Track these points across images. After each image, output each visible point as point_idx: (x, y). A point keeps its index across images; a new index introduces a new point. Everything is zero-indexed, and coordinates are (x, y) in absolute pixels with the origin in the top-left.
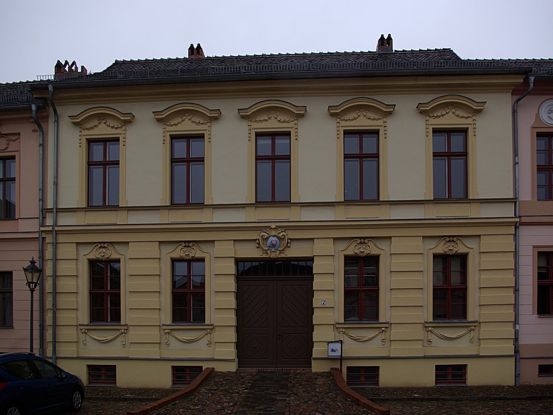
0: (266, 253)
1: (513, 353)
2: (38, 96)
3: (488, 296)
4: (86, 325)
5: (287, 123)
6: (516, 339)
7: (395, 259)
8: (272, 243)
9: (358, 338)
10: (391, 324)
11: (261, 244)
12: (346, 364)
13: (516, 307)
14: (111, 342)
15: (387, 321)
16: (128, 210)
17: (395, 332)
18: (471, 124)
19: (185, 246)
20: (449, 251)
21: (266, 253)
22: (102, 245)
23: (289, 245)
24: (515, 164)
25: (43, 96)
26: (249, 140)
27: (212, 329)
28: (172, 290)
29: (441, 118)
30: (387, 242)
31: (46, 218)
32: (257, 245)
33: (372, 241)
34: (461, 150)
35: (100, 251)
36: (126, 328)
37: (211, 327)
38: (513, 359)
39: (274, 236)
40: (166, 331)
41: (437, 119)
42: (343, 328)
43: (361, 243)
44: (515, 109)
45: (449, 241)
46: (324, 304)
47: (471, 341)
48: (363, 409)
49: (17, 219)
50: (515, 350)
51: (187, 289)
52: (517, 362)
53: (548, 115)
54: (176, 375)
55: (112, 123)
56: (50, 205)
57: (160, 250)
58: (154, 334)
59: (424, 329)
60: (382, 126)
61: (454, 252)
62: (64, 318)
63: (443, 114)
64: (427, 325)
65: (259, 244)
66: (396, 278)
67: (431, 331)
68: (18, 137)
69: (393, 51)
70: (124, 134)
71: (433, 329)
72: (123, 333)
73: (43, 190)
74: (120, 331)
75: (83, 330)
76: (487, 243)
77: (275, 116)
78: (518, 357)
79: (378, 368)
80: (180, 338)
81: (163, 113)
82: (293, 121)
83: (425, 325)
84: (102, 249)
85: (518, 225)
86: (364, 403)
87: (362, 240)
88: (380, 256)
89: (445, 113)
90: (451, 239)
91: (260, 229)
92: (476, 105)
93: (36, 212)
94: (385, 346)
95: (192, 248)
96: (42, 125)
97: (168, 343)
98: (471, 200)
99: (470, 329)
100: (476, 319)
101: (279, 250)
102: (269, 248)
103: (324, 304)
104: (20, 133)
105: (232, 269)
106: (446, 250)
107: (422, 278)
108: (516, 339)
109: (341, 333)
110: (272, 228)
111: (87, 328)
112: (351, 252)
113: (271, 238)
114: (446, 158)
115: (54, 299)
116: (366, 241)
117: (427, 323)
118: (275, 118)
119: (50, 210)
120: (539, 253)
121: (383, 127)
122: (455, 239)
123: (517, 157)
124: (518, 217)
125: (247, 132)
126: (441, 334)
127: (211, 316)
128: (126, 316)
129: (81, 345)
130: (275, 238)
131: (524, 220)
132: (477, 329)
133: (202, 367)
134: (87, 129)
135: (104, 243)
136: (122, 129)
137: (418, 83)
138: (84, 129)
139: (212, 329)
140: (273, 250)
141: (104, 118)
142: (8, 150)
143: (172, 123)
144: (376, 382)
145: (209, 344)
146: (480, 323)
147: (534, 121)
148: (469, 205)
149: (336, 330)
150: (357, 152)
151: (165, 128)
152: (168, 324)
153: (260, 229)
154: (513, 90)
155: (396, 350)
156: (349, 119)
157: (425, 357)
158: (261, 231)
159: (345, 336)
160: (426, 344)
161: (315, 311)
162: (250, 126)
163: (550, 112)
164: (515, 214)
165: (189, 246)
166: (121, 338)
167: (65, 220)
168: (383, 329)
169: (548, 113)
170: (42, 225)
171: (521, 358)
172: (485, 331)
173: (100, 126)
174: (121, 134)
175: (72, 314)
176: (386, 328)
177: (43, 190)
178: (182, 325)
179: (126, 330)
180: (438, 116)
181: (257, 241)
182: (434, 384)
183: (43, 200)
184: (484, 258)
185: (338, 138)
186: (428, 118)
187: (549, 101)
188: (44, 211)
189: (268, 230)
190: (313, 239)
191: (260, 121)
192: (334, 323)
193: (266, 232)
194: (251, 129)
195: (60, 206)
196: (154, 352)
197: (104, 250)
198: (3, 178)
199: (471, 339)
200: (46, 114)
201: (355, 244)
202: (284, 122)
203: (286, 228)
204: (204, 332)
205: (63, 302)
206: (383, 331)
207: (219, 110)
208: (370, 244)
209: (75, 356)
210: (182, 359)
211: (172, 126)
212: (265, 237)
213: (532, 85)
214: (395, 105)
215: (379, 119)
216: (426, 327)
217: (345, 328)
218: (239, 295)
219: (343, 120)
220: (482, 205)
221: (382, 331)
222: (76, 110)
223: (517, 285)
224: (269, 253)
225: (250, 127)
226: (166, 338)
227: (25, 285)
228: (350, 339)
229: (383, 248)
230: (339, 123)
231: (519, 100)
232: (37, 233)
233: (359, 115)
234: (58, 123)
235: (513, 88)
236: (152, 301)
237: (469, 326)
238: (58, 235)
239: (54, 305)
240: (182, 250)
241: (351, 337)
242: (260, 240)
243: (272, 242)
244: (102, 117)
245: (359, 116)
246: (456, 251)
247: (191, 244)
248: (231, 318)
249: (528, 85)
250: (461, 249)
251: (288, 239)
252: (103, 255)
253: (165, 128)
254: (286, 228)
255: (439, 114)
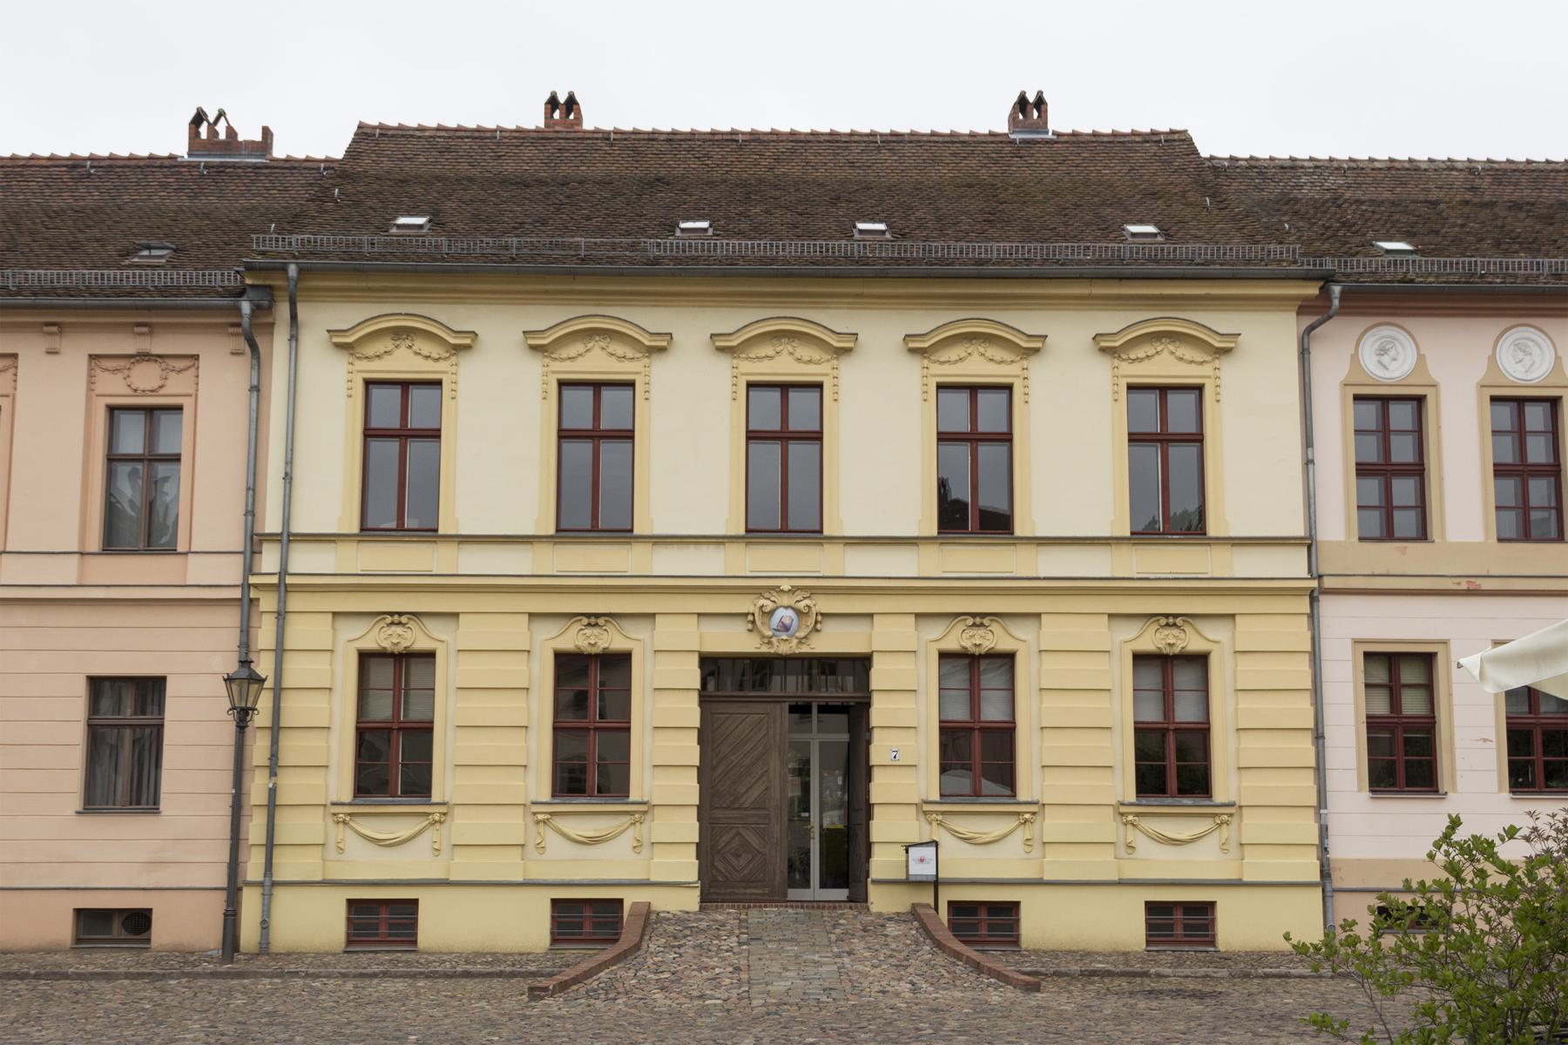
0: (769, 643)
1: (1317, 878)
2: (256, 282)
3: (1256, 748)
4: (349, 804)
5: (816, 364)
6: (1323, 849)
7: (1050, 662)
8: (782, 623)
9: (972, 835)
10: (1044, 805)
11: (758, 623)
12: (948, 894)
13: (1319, 774)
14: (413, 840)
15: (1035, 799)
16: (460, 542)
17: (1054, 825)
18: (1209, 377)
19: (589, 625)
20: (1168, 648)
21: (769, 643)
22: (396, 618)
23: (819, 626)
24: (1308, 462)
25: (268, 283)
26: (734, 399)
27: (645, 813)
28: (554, 722)
29: (1146, 361)
30: (1031, 625)
31: (261, 553)
32: (750, 626)
33: (999, 623)
34: (1193, 429)
35: (390, 632)
36: (445, 811)
37: (644, 808)
38: (1319, 891)
39: (786, 607)
40: (540, 817)
41: (1136, 364)
42: (937, 813)
43: (974, 625)
44: (1306, 346)
45: (1167, 625)
46: (895, 757)
47: (1224, 848)
48: (988, 979)
49: (186, 554)
50: (1322, 872)
51: (588, 721)
52: (1327, 899)
53: (1378, 358)
54: (558, 919)
55: (619, 349)
56: (272, 524)
57: (531, 633)
58: (512, 826)
59: (1119, 818)
60: (1018, 376)
61: (1177, 650)
62: (293, 786)
63: (1149, 354)
64: (1123, 809)
65: (753, 622)
66: (1052, 702)
67: (1133, 824)
68: (192, 363)
69: (1047, 133)
70: (452, 373)
71: (1136, 818)
72: (436, 822)
73: (254, 490)
74: (430, 817)
75: (340, 815)
76: (1250, 632)
77: (791, 350)
78: (1328, 888)
79: (1017, 904)
80: (572, 833)
81: (546, 335)
82: (828, 361)
83: (1120, 809)
84: (394, 628)
85: (1315, 594)
86: (989, 969)
87: (978, 620)
88: (1017, 653)
89: (1154, 352)
90: (1171, 620)
91: (758, 591)
92: (1219, 339)
93: (236, 540)
94: (1030, 856)
95: (604, 628)
96: (259, 340)
97: (542, 845)
98: (1211, 538)
99: (1219, 822)
100: (1232, 798)
101: (797, 638)
102: (777, 633)
103: (895, 757)
104: (198, 356)
105: (693, 678)
106: (1160, 646)
107: (1108, 706)
108: (1323, 849)
109: (934, 824)
110: (782, 591)
111: (349, 812)
112: (952, 644)
113: (781, 613)
114: (1159, 445)
115: (275, 742)
116: (986, 621)
117: (1123, 804)
118: (791, 354)
119: (273, 538)
120: (1368, 656)
121: (1021, 378)
122: (1179, 621)
123: (1310, 449)
124: (1314, 579)
125: (728, 381)
126: (1158, 831)
127: (642, 782)
128: (444, 783)
129: (332, 853)
130: (790, 613)
131: (1329, 583)
132: (1235, 820)
133: (620, 901)
134: (367, 358)
135: (400, 614)
136: (448, 363)
137: (371, 284)
138: (358, 358)
139: (645, 813)
140: (785, 637)
141: (408, 336)
142: (162, 392)
143: (564, 355)
144: (1012, 939)
145: (638, 846)
146: (1240, 807)
147: (1347, 371)
148: (1209, 548)
149: (922, 817)
150: (965, 427)
151: (548, 366)
152: (544, 800)
153: (758, 591)
154: (1300, 307)
155: (1057, 865)
156: (947, 359)
157: (1121, 883)
158: (757, 596)
159: (942, 830)
160: (1122, 852)
161: (876, 773)
162: (737, 368)
163: (1382, 353)
164: (1310, 571)
165: (596, 625)
166: (430, 835)
167: (305, 560)
168: (1027, 816)
169: (1377, 355)
170: (249, 570)
171: (1334, 891)
172: (1253, 825)
173: (398, 352)
174: (446, 372)
175: (315, 778)
176: (1034, 813)
177: (253, 489)
178: (578, 802)
179: (444, 814)
180: (1138, 358)
181: (750, 618)
182: (1144, 946)
183: (251, 513)
184: (1245, 663)
185: (925, 400)
186: (1116, 362)
187: (1362, 341)
188: (255, 542)
189: (775, 594)
190: (871, 615)
191: (757, 358)
192: (917, 802)
193: (769, 599)
194: (739, 376)
195: (297, 528)
196: (509, 867)
197: (399, 630)
198: (144, 455)
199: (1223, 844)
200: (270, 320)
201: (961, 627)
202: (810, 361)
203: (813, 591)
204: (626, 820)
205: (294, 748)
206: (1026, 821)
207: (671, 334)
208: (995, 627)
209: (319, 878)
210: (576, 882)
211: (563, 360)
212: (768, 609)
213: (1336, 303)
214: (1047, 336)
215: (1012, 361)
216: (1122, 814)
217: (943, 813)
218: (705, 736)
219: (935, 362)
220: (1234, 548)
221: (1025, 822)
222: (347, 315)
223: (1320, 726)
224: (776, 643)
225: (735, 370)
226: (540, 833)
227: (260, 714)
228: (952, 837)
229: (1022, 637)
230: (927, 368)
231: (1312, 328)
232: (237, 588)
233: (969, 352)
234: (297, 340)
235: (1300, 303)
236: (509, 747)
237: (1216, 814)
238: (289, 594)
239: (274, 756)
240: (582, 632)
241: (954, 833)
242: (756, 615)
243: (783, 620)
244: (400, 334)
245: (970, 354)
246: (1183, 648)
247: (601, 621)
248: (688, 788)
249: (1330, 300)
250: (1194, 644)
251: (817, 614)
252: (395, 641)
253: (548, 366)
254: (813, 591)
255: (1141, 354)
